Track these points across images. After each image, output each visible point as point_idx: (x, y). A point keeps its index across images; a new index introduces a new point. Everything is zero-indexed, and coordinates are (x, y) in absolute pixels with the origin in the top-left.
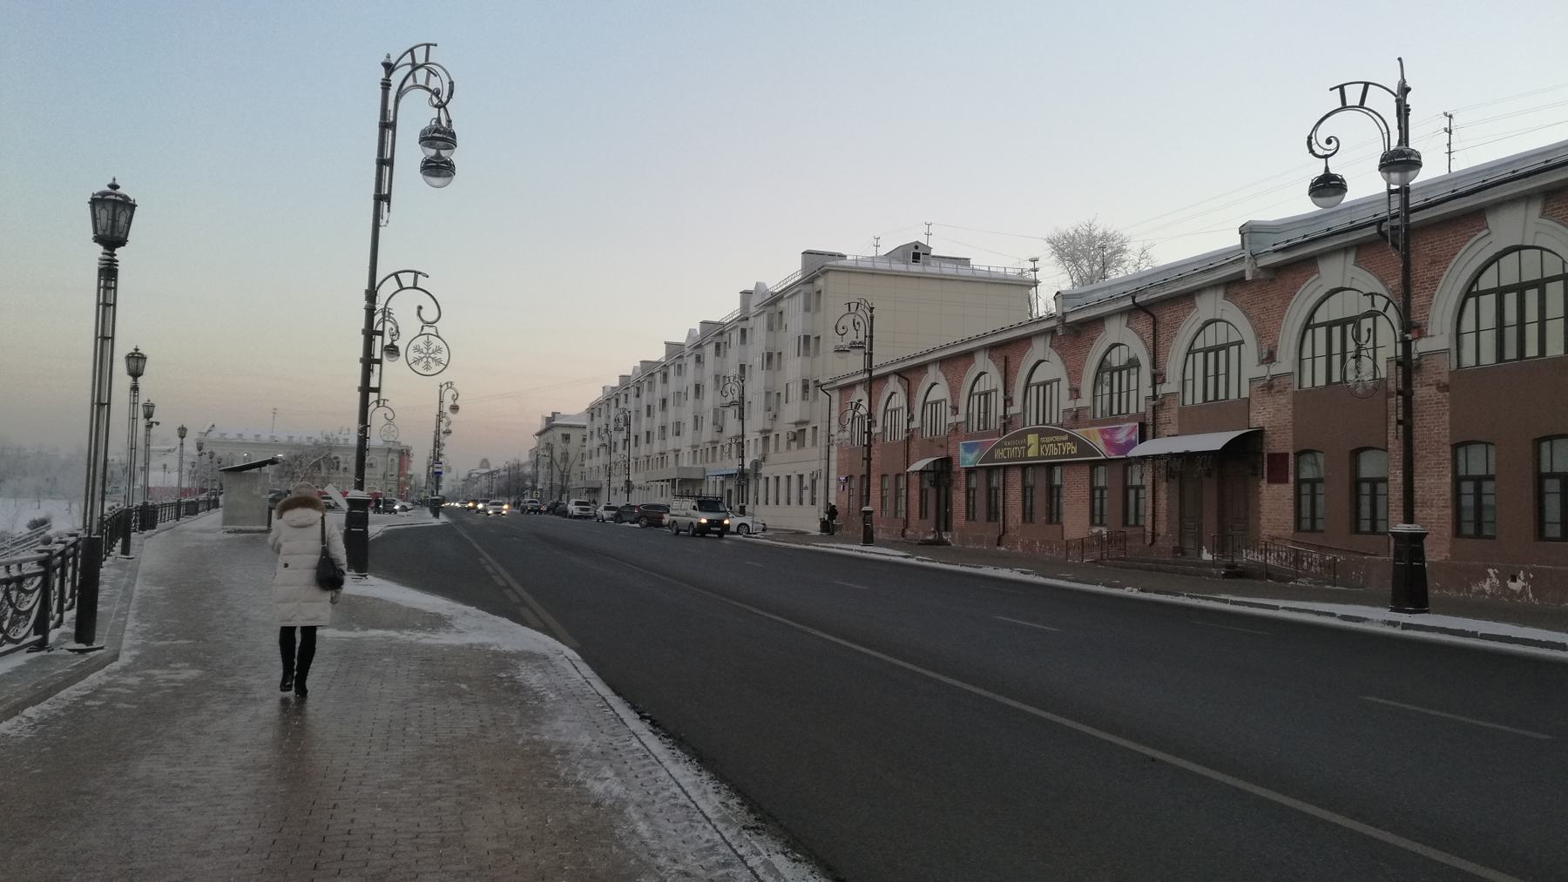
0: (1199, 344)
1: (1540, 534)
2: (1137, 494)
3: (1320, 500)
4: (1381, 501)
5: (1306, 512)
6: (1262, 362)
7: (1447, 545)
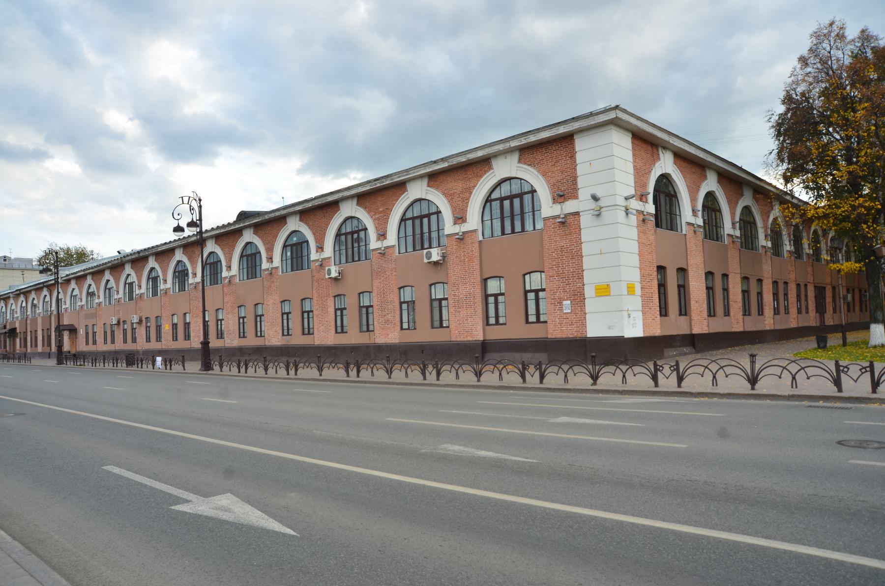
0: (409, 215)
1: (527, 322)
2: (537, 299)
3: (501, 307)
4: (370, 316)
6: (378, 239)
7: (705, 323)
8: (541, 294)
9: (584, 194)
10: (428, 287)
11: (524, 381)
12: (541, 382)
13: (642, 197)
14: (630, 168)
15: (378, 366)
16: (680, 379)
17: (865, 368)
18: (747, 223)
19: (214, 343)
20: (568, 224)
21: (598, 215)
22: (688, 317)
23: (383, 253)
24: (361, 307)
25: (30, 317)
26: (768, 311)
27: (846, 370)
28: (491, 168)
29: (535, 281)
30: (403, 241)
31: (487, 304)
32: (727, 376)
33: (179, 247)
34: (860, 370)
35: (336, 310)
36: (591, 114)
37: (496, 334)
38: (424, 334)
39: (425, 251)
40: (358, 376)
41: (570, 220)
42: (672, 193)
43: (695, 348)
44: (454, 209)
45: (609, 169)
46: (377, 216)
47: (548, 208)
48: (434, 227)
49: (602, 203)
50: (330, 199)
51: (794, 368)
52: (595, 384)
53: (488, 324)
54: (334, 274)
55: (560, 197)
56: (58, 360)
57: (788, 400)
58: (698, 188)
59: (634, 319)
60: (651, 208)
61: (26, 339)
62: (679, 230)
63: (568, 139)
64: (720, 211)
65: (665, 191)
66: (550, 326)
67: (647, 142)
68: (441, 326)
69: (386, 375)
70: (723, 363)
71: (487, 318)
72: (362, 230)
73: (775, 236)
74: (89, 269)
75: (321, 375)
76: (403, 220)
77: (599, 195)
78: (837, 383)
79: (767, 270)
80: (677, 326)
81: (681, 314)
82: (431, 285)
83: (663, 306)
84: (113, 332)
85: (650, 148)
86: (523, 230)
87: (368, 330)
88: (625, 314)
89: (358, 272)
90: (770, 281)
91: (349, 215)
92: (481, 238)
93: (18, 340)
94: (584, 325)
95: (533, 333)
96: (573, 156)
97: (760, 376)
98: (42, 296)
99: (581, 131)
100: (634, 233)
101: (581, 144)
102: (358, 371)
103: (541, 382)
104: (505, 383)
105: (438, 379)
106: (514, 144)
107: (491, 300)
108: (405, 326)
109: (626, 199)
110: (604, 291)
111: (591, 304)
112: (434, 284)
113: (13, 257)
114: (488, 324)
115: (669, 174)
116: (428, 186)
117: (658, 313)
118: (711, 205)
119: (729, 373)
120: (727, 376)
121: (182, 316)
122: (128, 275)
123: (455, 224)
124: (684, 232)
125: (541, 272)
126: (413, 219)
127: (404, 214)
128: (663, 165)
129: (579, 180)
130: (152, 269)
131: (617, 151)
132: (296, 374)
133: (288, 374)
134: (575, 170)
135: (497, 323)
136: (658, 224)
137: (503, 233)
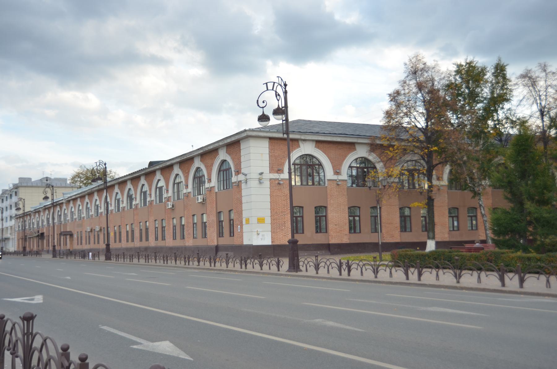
19: (113, 245)
25: (63, 223)
33: (198, 155)
42: (317, 162)
49: (248, 177)
56: (106, 256)
61: (49, 240)
70: (331, 261)
74: (79, 194)
75: (317, 273)
81: (317, 232)
83: (221, 231)
84: (98, 235)
92: (217, 190)
93: (45, 241)
98: (114, 194)
101: (243, 145)
104: (394, 280)
113: (52, 178)
121: (179, 219)
122: (177, 175)
130: (224, 161)
137: (224, 189)
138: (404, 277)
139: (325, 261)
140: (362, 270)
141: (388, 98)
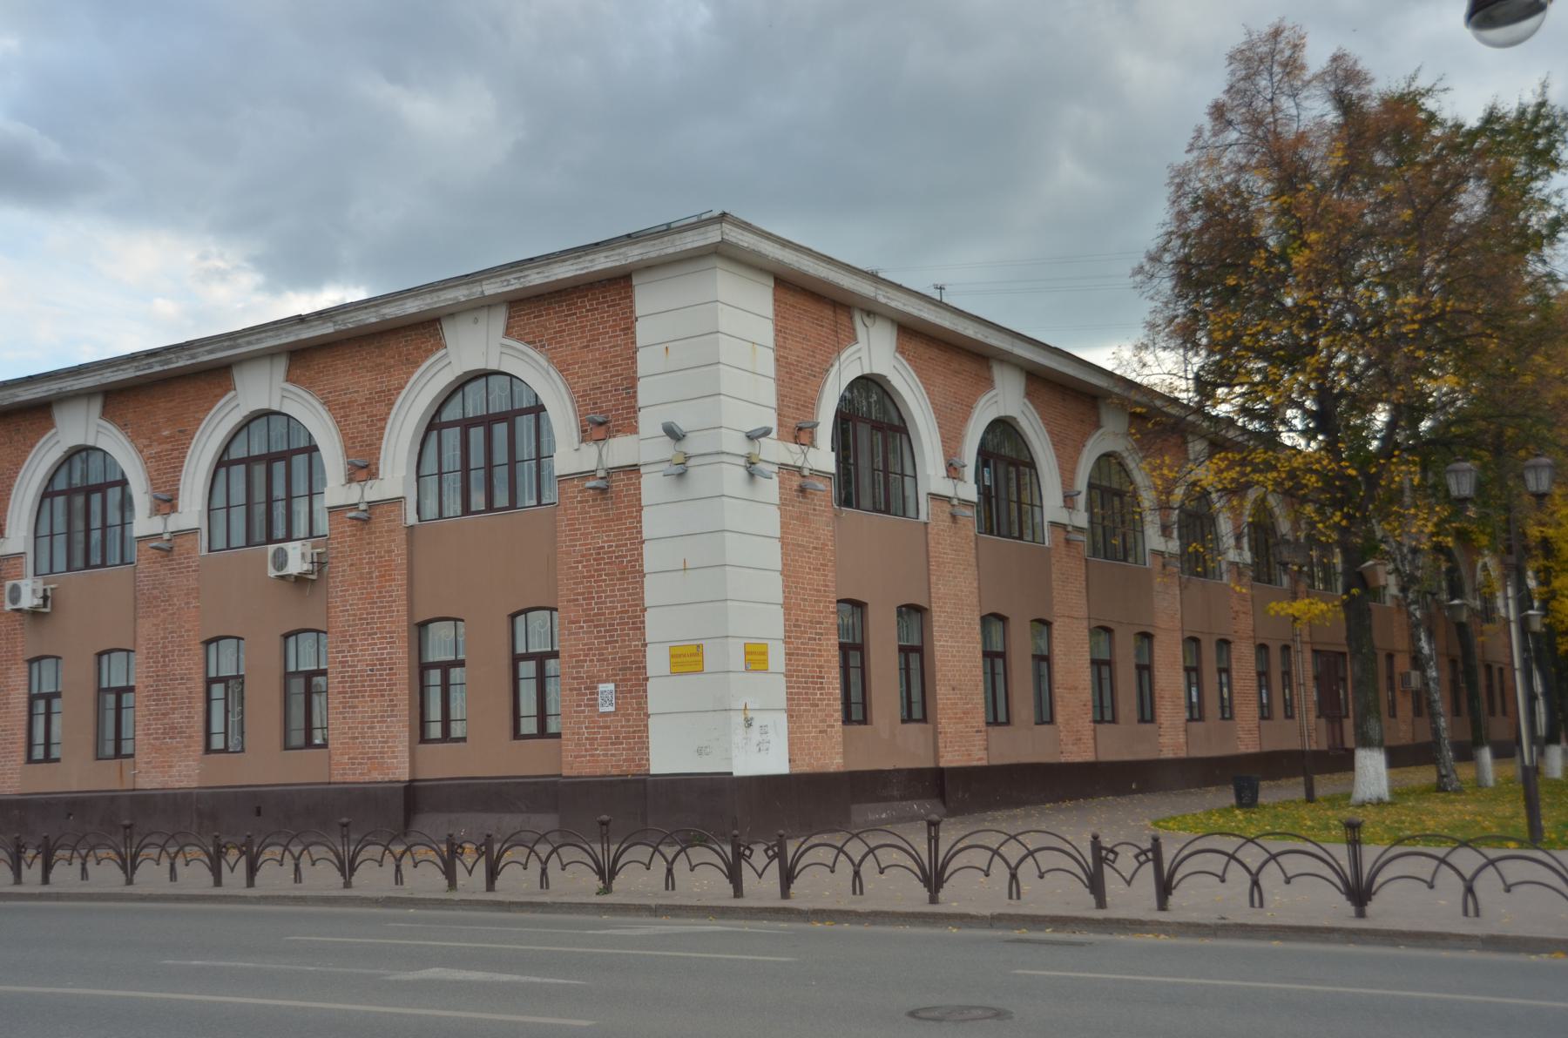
0: (238, 451)
1: (517, 734)
2: (541, 679)
4: (127, 715)
5: (39, 737)
7: (979, 740)
8: (551, 665)
9: (650, 422)
10: (278, 641)
11: (452, 884)
12: (490, 886)
13: (801, 434)
14: (766, 362)
15: (102, 853)
16: (1165, 888)
17: (1144, 852)
18: (1110, 495)
20: (614, 491)
21: (681, 475)
22: (929, 726)
23: (168, 548)
24: (101, 691)
26: (1171, 711)
27: (1111, 856)
28: (440, 344)
29: (536, 634)
30: (431, 484)
31: (423, 687)
32: (1508, 889)
34: (1137, 857)
35: (32, 699)
36: (667, 230)
37: (441, 764)
38: (265, 765)
39: (272, 548)
40: (45, 880)
41: (619, 483)
42: (896, 422)
43: (944, 803)
44: (583, 400)
45: (715, 358)
46: (155, 449)
47: (570, 454)
48: (526, 449)
49: (692, 446)
50: (26, 395)
51: (1253, 857)
52: (607, 890)
53: (424, 739)
54: (28, 601)
55: (597, 428)
57: (991, 926)
58: (967, 409)
59: (764, 730)
60: (823, 458)
62: (911, 511)
63: (619, 283)
64: (1032, 465)
65: (870, 420)
66: (568, 744)
67: (816, 303)
68: (309, 743)
69: (120, 876)
70: (1032, 841)
71: (423, 723)
72: (114, 484)
73: (1196, 522)
76: (223, 462)
77: (682, 424)
78: (1096, 885)
79: (1168, 611)
80: (892, 745)
81: (908, 718)
82: (286, 636)
83: (856, 695)
85: (828, 313)
86: (513, 505)
87: (118, 754)
88: (739, 719)
89: (98, 599)
90: (1178, 637)
91: (263, 404)
92: (412, 519)
94: (644, 745)
95: (529, 761)
96: (629, 330)
97: (1178, 876)
99: (649, 267)
100: (771, 521)
101: (647, 299)
102: (47, 868)
103: (490, 886)
105: (250, 883)
106: (491, 288)
107: (435, 676)
108: (218, 742)
109: (751, 437)
110: (688, 660)
111: (661, 693)
112: (296, 633)
114: (424, 739)
115: (883, 377)
116: (288, 379)
117: (838, 715)
118: (1003, 453)
119: (1022, 867)
120: (1508, 889)
123: (350, 480)
124: (923, 517)
125: (553, 610)
126: (248, 461)
127: (226, 448)
128: (864, 354)
129: (642, 386)
131: (727, 320)
132: (45, 880)
133: (18, 879)
134: (634, 361)
135: (446, 736)
136: (847, 497)
137: (466, 510)
138: (443, 881)
139: (993, 840)
140: (544, 872)
141: (1165, 176)
